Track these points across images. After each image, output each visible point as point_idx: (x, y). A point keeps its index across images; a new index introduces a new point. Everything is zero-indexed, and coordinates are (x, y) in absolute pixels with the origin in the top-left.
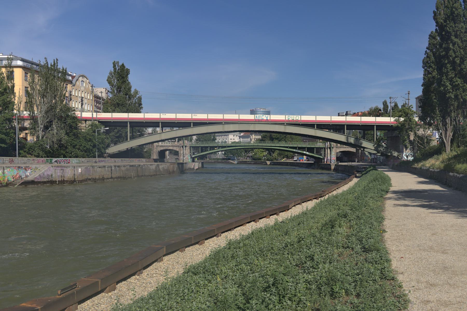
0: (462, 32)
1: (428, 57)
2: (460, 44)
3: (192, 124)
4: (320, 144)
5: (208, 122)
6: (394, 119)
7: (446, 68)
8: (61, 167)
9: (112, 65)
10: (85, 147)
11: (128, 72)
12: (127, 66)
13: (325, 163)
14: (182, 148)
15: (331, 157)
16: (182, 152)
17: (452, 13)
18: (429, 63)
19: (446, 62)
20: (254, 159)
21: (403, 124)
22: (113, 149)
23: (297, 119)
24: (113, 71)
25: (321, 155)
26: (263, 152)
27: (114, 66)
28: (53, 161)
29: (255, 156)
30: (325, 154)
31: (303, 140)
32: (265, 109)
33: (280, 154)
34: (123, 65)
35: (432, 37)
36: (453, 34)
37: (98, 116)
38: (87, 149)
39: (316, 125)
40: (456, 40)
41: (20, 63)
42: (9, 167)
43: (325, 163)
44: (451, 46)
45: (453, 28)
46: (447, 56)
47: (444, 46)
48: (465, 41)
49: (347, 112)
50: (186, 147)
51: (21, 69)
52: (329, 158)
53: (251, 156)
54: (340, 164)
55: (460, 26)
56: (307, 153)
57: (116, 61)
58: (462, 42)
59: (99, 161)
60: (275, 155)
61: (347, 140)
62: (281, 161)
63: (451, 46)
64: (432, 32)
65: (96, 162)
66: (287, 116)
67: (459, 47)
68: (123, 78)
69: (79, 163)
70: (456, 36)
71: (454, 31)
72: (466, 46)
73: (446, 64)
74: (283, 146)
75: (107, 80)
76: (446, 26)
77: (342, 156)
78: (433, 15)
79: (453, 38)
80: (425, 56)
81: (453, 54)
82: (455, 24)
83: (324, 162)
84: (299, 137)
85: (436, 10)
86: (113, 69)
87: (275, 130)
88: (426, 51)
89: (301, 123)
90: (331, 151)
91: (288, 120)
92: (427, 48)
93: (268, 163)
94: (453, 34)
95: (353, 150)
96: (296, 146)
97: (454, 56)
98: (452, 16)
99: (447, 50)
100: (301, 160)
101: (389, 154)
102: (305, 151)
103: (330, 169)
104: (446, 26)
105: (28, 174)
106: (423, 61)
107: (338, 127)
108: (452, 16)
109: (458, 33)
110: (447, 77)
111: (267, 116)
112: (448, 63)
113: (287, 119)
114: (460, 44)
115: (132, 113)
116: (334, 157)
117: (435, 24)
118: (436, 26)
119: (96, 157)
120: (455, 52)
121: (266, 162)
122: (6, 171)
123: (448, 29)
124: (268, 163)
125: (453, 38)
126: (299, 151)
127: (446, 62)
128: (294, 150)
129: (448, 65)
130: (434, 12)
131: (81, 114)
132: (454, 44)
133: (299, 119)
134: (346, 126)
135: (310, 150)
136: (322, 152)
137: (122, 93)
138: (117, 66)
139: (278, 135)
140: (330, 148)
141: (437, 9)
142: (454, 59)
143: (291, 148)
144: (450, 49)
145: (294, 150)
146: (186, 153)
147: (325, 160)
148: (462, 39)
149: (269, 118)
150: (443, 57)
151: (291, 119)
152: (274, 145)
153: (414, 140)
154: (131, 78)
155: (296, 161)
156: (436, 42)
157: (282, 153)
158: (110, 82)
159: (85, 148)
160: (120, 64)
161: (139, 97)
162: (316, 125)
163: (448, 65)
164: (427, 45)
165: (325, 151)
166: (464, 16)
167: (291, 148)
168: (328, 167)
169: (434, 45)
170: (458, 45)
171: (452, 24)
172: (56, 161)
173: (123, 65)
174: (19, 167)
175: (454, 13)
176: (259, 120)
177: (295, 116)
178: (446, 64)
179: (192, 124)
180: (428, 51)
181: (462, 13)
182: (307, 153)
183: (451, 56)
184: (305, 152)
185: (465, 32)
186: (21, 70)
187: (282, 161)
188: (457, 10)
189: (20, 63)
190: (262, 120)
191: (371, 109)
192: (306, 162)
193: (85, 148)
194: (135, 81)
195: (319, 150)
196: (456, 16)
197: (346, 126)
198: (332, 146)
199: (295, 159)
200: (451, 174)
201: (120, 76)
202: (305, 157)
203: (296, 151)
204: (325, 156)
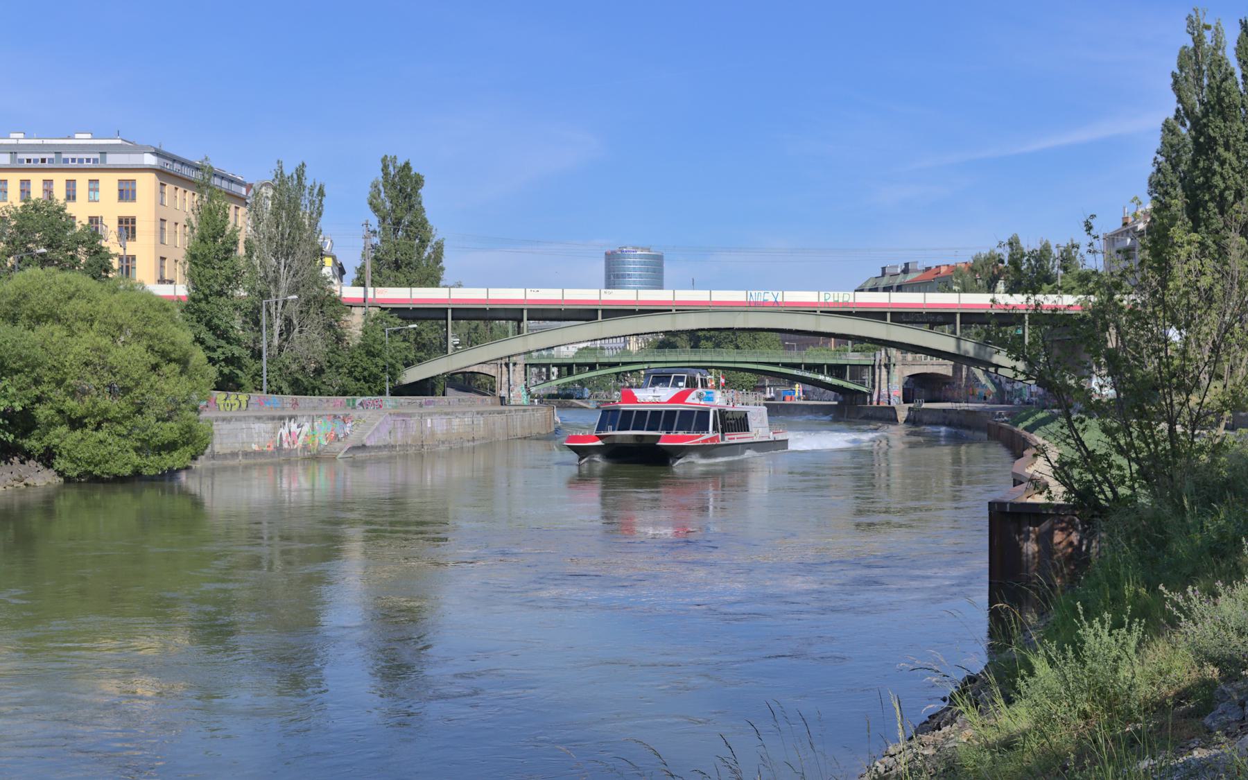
1: (1159, 170)
2: (1235, 163)
3: (600, 313)
4: (853, 358)
5: (637, 308)
8: (403, 415)
9: (381, 166)
10: (365, 369)
11: (419, 181)
13: (875, 404)
14: (504, 368)
16: (505, 379)
17: (1220, 100)
18: (1162, 186)
19: (1207, 198)
25: (863, 384)
30: (873, 380)
31: (784, 341)
36: (1221, 141)
37: (378, 296)
41: (150, 160)
42: (320, 416)
43: (875, 404)
44: (1216, 166)
46: (1207, 186)
47: (1201, 165)
48: (1245, 157)
49: (907, 265)
50: (515, 364)
52: (884, 391)
55: (1236, 128)
57: (390, 154)
58: (1239, 158)
61: (958, 347)
63: (1216, 166)
64: (1167, 121)
66: (822, 294)
67: (1233, 169)
71: (1223, 136)
72: (1246, 168)
74: (766, 360)
76: (1206, 125)
77: (919, 386)
78: (1172, 81)
79: (1221, 150)
80: (1154, 169)
83: (871, 402)
84: (777, 336)
85: (1178, 72)
89: (854, 310)
94: (1221, 141)
96: (799, 361)
97: (1222, 186)
98: (1219, 106)
99: (1208, 172)
100: (788, 397)
103: (894, 420)
104: (1206, 125)
105: (347, 430)
107: (940, 319)
108: (1219, 106)
111: (775, 293)
113: (822, 300)
114: (1235, 163)
115: (428, 286)
116: (897, 390)
117: (1175, 98)
120: (1224, 179)
125: (1221, 150)
127: (1207, 198)
128: (795, 372)
129: (1211, 205)
130: (1174, 75)
131: (366, 292)
132: (1222, 163)
133: (851, 300)
136: (867, 377)
138: (391, 168)
141: (1181, 68)
143: (785, 365)
144: (1214, 173)
145: (795, 372)
147: (875, 397)
149: (779, 299)
150: (1199, 187)
151: (831, 300)
155: (772, 399)
163: (1211, 205)
164: (1158, 145)
166: (1243, 106)
167: (785, 365)
168: (887, 416)
169: (1172, 146)
173: (407, 166)
174: (335, 416)
176: (756, 304)
177: (841, 294)
179: (600, 313)
180: (1161, 159)
183: (1216, 187)
184: (821, 377)
185: (1246, 140)
186: (152, 177)
188: (1228, 94)
189: (150, 160)
190: (765, 304)
192: (802, 402)
193: (366, 373)
195: (857, 370)
197: (958, 316)
198: (893, 360)
199: (768, 396)
201: (400, 192)
202: (798, 387)
204: (874, 387)
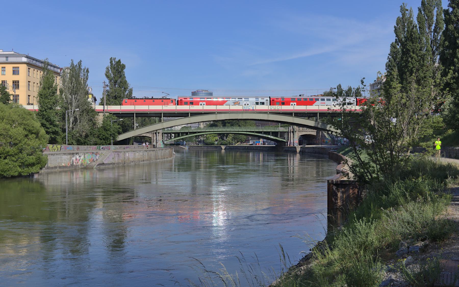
1: (389, 61)
2: (417, 59)
6: (360, 107)
7: (406, 75)
8: (118, 152)
11: (124, 67)
13: (289, 146)
19: (406, 71)
20: (207, 144)
25: (284, 139)
27: (111, 62)
30: (288, 137)
31: (256, 124)
33: (234, 139)
34: (119, 60)
35: (393, 46)
36: (411, 50)
41: (24, 60)
43: (289, 146)
44: (410, 59)
46: (406, 66)
47: (404, 59)
51: (25, 65)
52: (292, 141)
56: (272, 137)
57: (113, 57)
60: (229, 139)
63: (410, 59)
64: (392, 43)
67: (416, 60)
69: (115, 149)
70: (413, 53)
73: (406, 72)
76: (406, 45)
77: (304, 139)
78: (394, 29)
80: (388, 61)
83: (287, 145)
84: (254, 122)
85: (396, 26)
86: (110, 64)
90: (293, 134)
94: (411, 50)
95: (314, 132)
96: (262, 131)
97: (412, 66)
99: (407, 61)
100: (257, 144)
102: (270, 135)
105: (97, 158)
110: (406, 81)
113: (270, 109)
116: (296, 141)
120: (412, 64)
125: (411, 54)
126: (264, 135)
127: (406, 71)
128: (260, 135)
132: (412, 58)
133: (280, 109)
135: (275, 134)
136: (286, 136)
137: (118, 88)
139: (229, 121)
140: (293, 132)
141: (397, 24)
144: (409, 62)
145: (260, 135)
149: (254, 108)
151: (273, 109)
152: (221, 130)
155: (252, 144)
157: (236, 136)
158: (107, 76)
159: (104, 137)
160: (117, 60)
173: (119, 60)
174: (93, 153)
175: (412, 35)
176: (246, 110)
180: (390, 57)
183: (410, 67)
187: (236, 145)
189: (24, 60)
193: (104, 137)
195: (282, 134)
198: (295, 130)
199: (250, 143)
200: (418, 148)
203: (262, 135)
204: (288, 140)
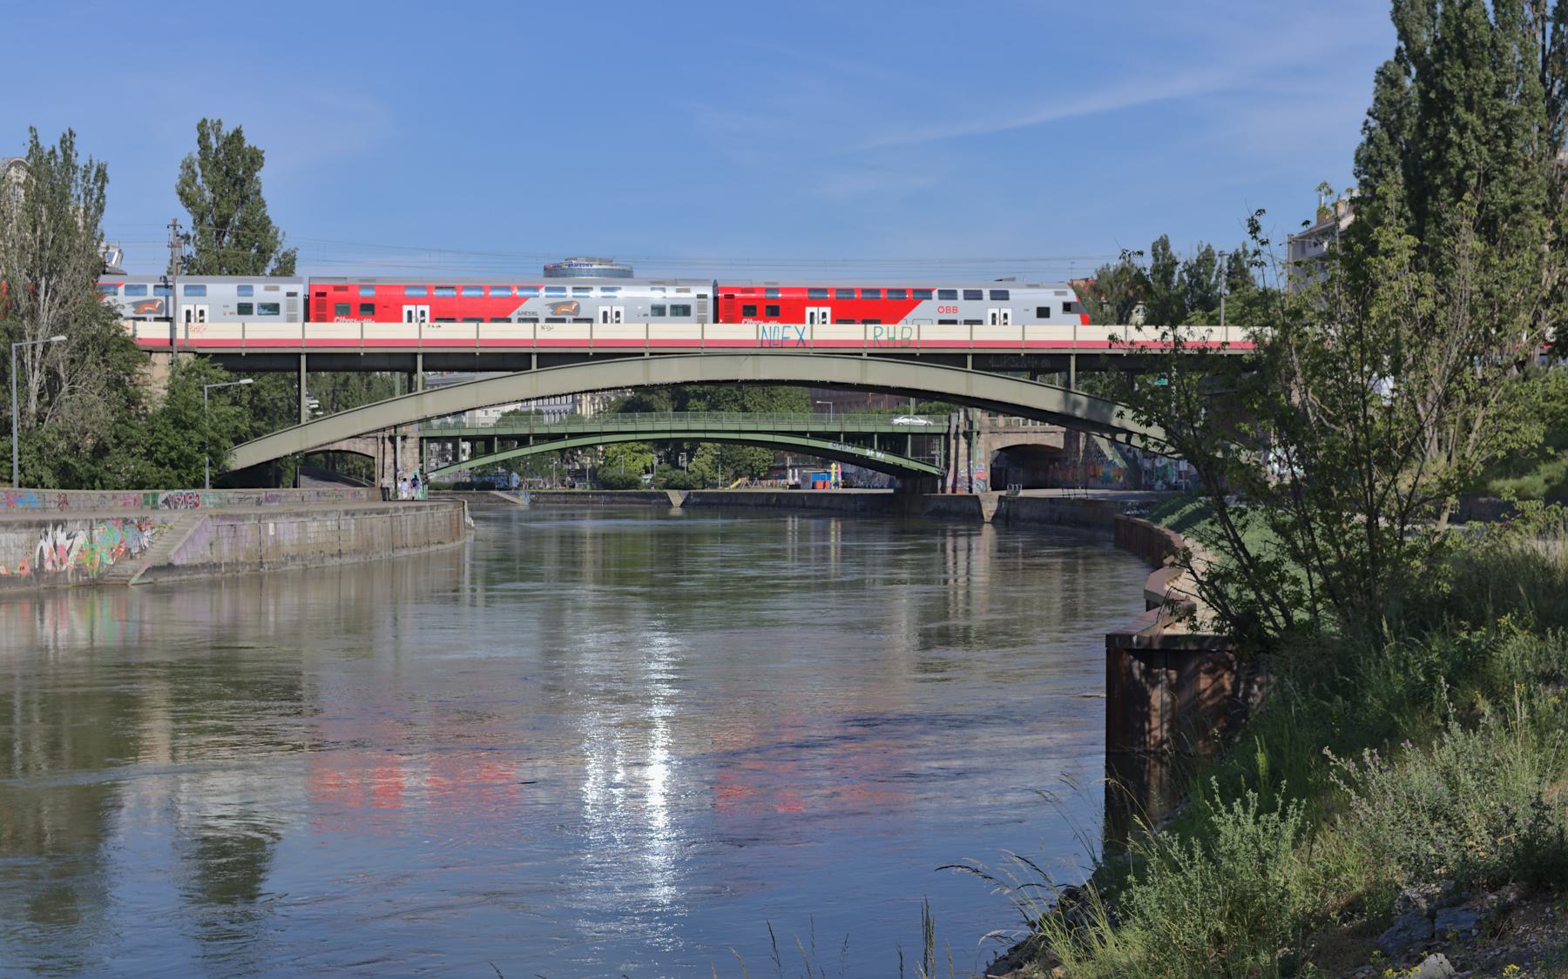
0: (1485, 95)
1: (1370, 140)
2: (1481, 130)
3: (534, 358)
5: (591, 351)
8: (232, 517)
11: (255, 159)
12: (250, 141)
13: (949, 491)
14: (388, 445)
15: (972, 469)
17: (1461, 34)
19: (1438, 181)
20: (607, 484)
21: (1274, 349)
22: (245, 457)
23: (906, 336)
24: (196, 156)
25: (931, 462)
26: (641, 452)
27: (203, 140)
28: (159, 502)
29: (612, 473)
31: (814, 399)
32: (610, 262)
33: (721, 462)
34: (238, 132)
35: (1386, 79)
36: (1461, 96)
38: (181, 455)
39: (970, 359)
40: (1471, 118)
42: (103, 521)
43: (949, 491)
44: (1453, 134)
45: (1460, 79)
46: (1440, 164)
50: (404, 438)
52: (963, 472)
53: (594, 471)
54: (1022, 493)
56: (880, 456)
57: (212, 117)
58: (1486, 122)
59: (267, 500)
60: (701, 463)
62: (726, 490)
65: (259, 503)
67: (1478, 138)
68: (240, 182)
70: (1469, 107)
73: (1438, 187)
75: (181, 194)
76: (1439, 73)
77: (1014, 465)
79: (1460, 110)
80: (1363, 139)
81: (1459, 159)
82: (1467, 68)
83: (944, 489)
84: (806, 392)
87: (828, 379)
88: (1366, 122)
89: (918, 352)
90: (969, 445)
91: (893, 340)
92: (1369, 114)
93: (676, 497)
96: (836, 428)
97: (1461, 163)
99: (1443, 142)
100: (820, 484)
101: (1219, 455)
102: (872, 447)
104: (1439, 73)
105: (145, 541)
106: (1357, 155)
107: (1046, 364)
109: (1475, 97)
112: (1443, 184)
113: (870, 337)
114: (1481, 130)
118: (1400, 38)
119: (203, 486)
121: (666, 496)
122: (95, 532)
123: (1447, 84)
124: (676, 497)
125: (1460, 110)
126: (849, 449)
127: (1438, 181)
128: (830, 445)
129: (1445, 191)
131: (173, 330)
132: (1462, 129)
133: (914, 337)
134: (1073, 359)
136: (938, 451)
138: (213, 139)
140: (968, 436)
142: (1461, 173)
144: (1450, 144)
145: (830, 445)
146: (404, 465)
148: (1485, 114)
149: (806, 337)
151: (884, 337)
152: (683, 427)
153: (1302, 403)
154: (266, 178)
155: (797, 486)
156: (1397, 97)
157: (732, 452)
158: (187, 200)
159: (174, 454)
160: (227, 130)
161: (285, 255)
162: (970, 359)
164: (1369, 103)
165: (948, 447)
169: (1391, 104)
170: (1473, 131)
171: (1458, 68)
172: (166, 501)
173: (238, 132)
174: (126, 521)
178: (1438, 187)
179: (534, 358)
180: (1373, 123)
181: (1487, 39)
182: (880, 456)
184: (869, 453)
187: (732, 488)
188: (1472, 26)
190: (783, 344)
191: (1102, 274)
192: (841, 490)
193: (174, 454)
194: (278, 191)
195: (922, 441)
196: (1472, 46)
197: (1073, 359)
198: (976, 426)
199: (791, 482)
200: (1482, 500)
202: (835, 468)
203: (838, 447)
204: (947, 466)
